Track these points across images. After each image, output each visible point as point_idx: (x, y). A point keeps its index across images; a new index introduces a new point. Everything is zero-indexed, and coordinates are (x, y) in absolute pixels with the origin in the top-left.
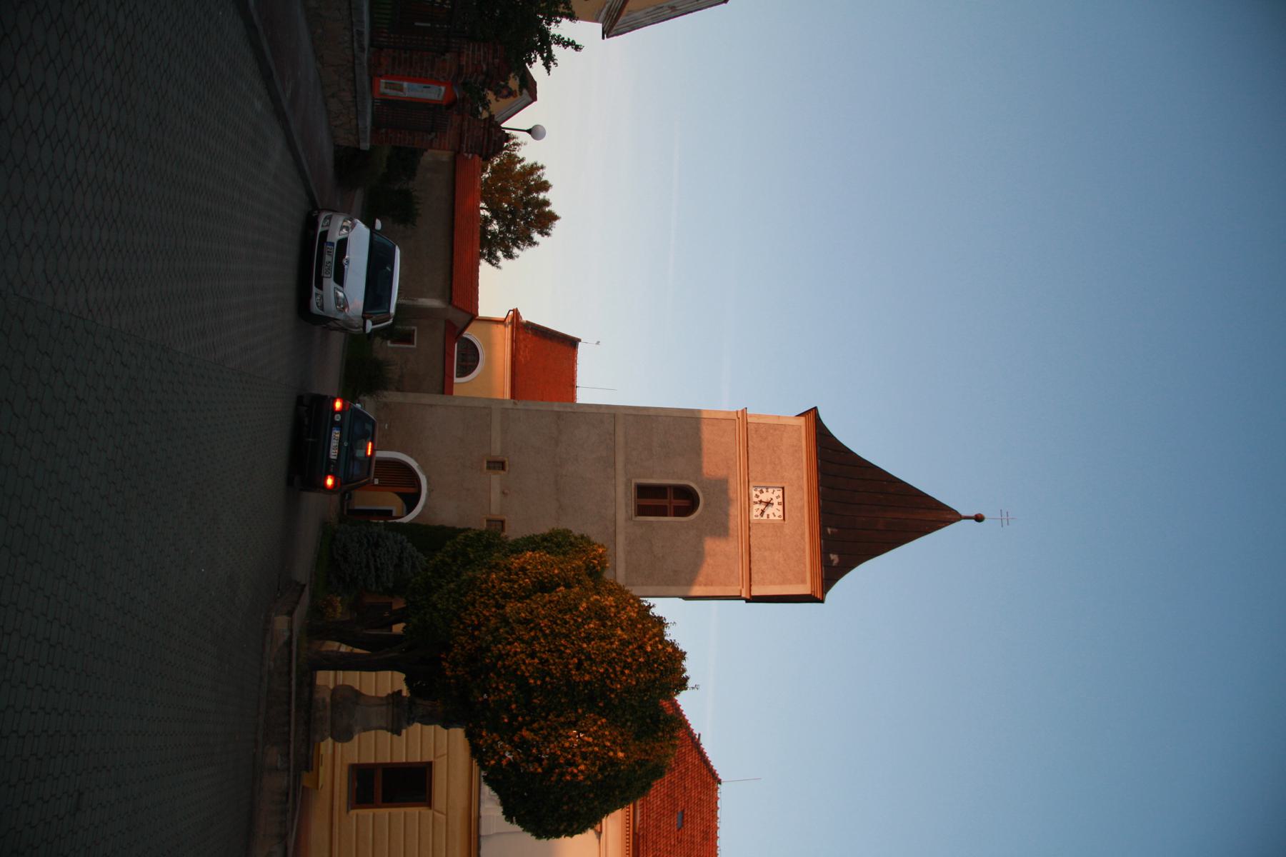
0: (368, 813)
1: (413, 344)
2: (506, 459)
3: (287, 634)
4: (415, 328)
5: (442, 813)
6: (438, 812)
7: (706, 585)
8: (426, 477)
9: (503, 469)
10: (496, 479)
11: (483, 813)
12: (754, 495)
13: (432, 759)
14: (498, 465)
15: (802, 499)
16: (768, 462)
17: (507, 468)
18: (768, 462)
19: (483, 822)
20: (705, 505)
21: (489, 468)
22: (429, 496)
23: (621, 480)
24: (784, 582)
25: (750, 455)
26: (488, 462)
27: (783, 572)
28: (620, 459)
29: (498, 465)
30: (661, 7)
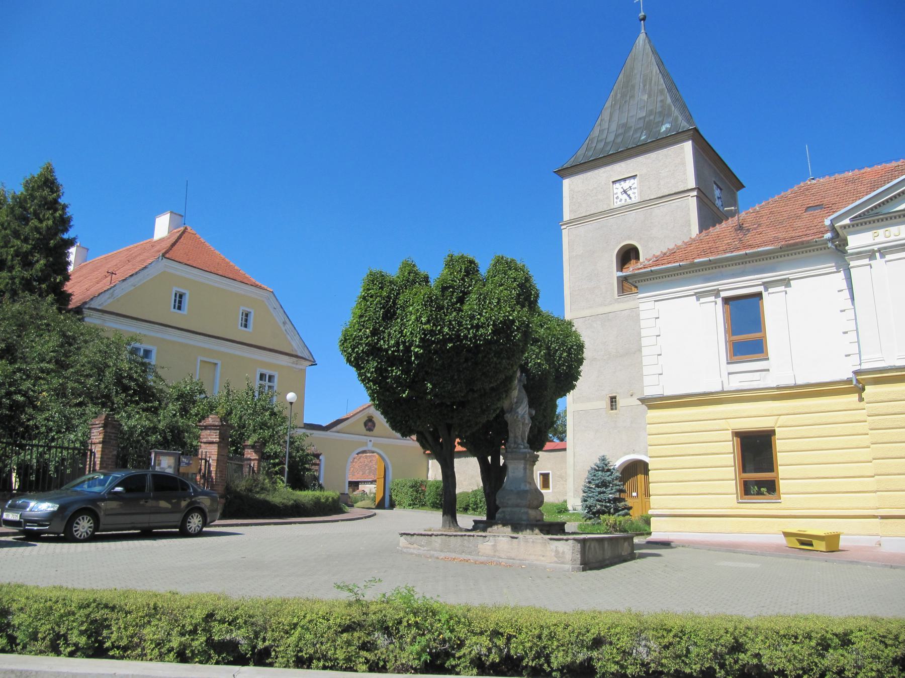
0: (783, 485)
1: (549, 474)
2: (608, 396)
3: (382, 495)
4: (550, 472)
5: (778, 419)
6: (776, 423)
7: (690, 226)
8: (624, 456)
9: (615, 398)
10: (621, 402)
11: (775, 385)
12: (620, 203)
13: (730, 432)
14: (613, 400)
15: (604, 172)
16: (596, 198)
17: (614, 395)
18: (596, 198)
19: (783, 383)
20: (630, 238)
21: (616, 409)
22: (638, 453)
23: (617, 307)
24: (683, 164)
25: (592, 213)
26: (612, 409)
27: (676, 166)
28: (601, 310)
29: (613, 400)
30: (286, 331)
